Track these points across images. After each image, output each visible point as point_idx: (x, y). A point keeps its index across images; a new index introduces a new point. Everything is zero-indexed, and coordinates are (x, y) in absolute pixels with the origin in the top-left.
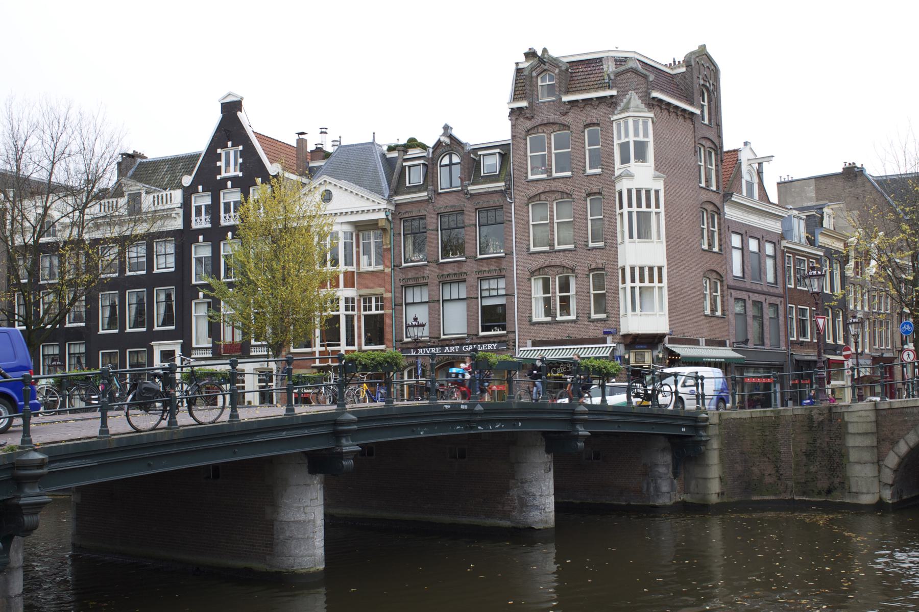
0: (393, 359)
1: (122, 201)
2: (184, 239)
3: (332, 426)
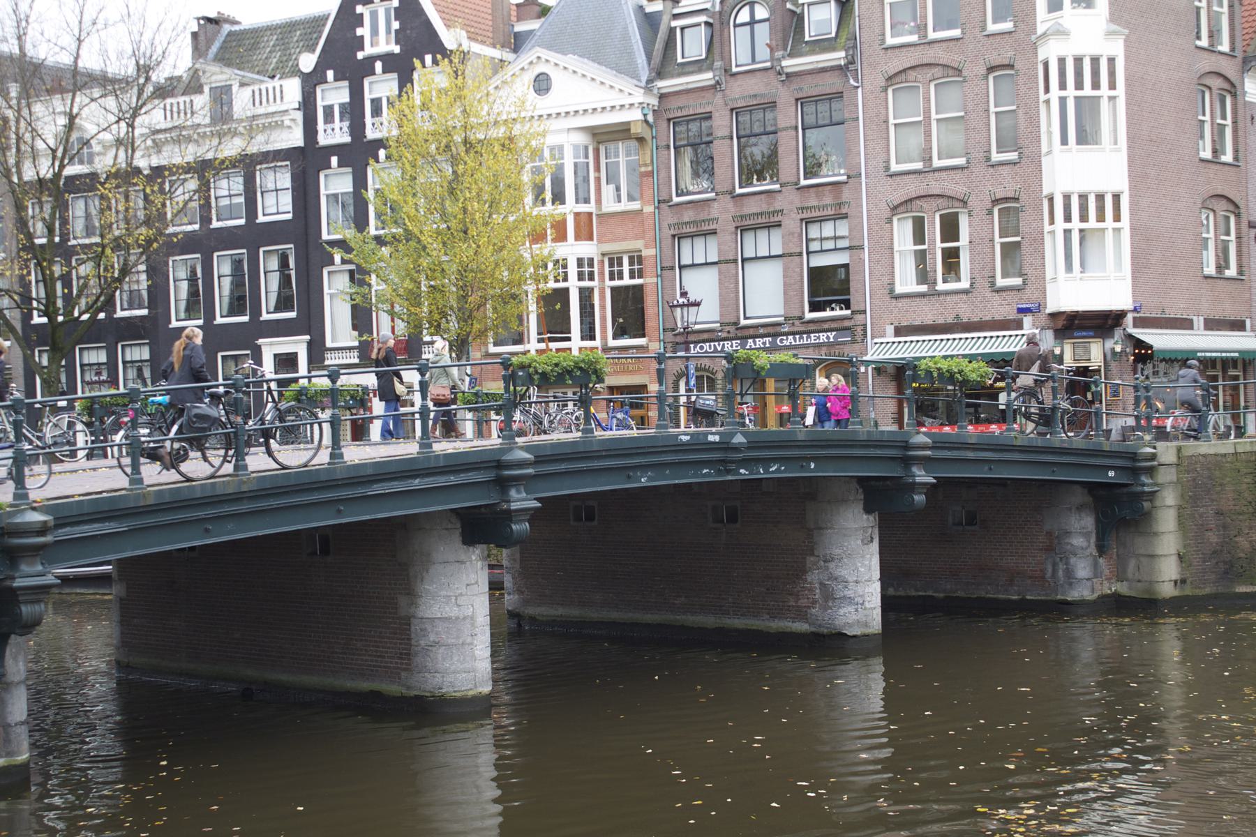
0: (590, 363)
1: (201, 101)
2: (307, 162)
3: (497, 471)
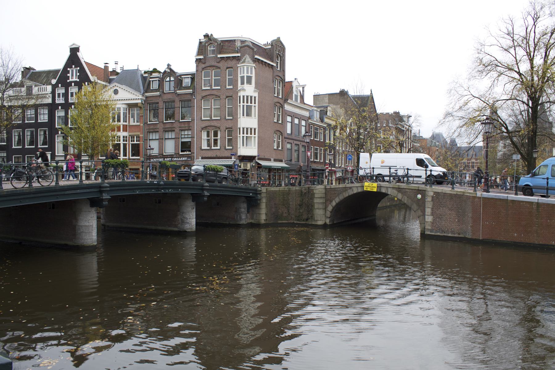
1: (23, 89)
2: (52, 108)
3: (99, 188)
